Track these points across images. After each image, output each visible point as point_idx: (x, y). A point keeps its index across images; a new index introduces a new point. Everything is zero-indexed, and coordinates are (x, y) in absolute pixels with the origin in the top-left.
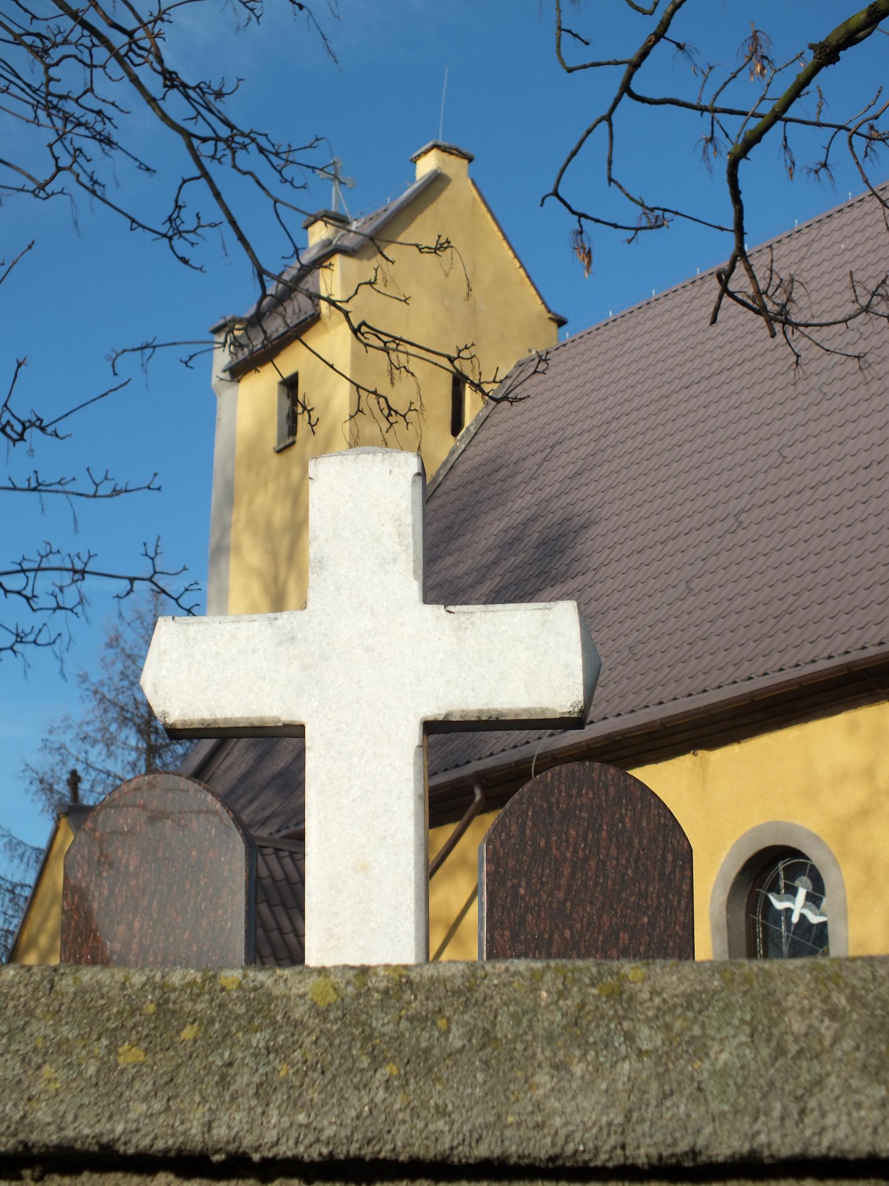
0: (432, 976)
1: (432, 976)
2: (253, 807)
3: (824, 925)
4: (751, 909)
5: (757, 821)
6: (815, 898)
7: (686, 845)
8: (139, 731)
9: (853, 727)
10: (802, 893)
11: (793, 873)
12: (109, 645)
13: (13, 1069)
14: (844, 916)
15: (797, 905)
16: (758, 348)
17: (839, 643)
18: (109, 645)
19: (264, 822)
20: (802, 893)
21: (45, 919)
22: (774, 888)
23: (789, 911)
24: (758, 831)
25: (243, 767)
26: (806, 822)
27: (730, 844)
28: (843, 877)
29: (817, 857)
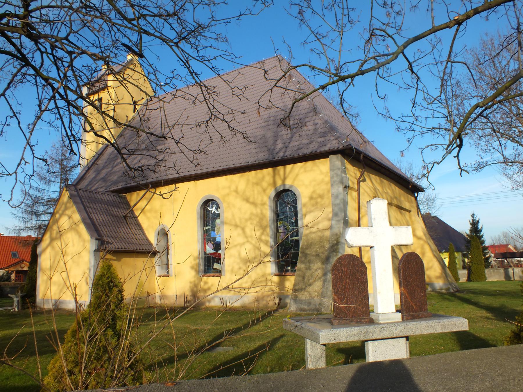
0: (513, 332)
1: (513, 332)
2: (97, 185)
3: (219, 214)
4: (204, 210)
5: (207, 194)
6: (217, 209)
7: (441, 313)
8: (60, 164)
9: (227, 179)
10: (214, 208)
11: (212, 204)
12: (52, 147)
13: (434, 304)
14: (223, 212)
15: (213, 210)
16: (229, 100)
17: (224, 164)
18: (52, 147)
19: (101, 188)
20: (214, 208)
21: (61, 208)
22: (209, 206)
23: (212, 211)
24: (207, 196)
25: (93, 176)
26: (216, 195)
27: (201, 198)
28: (224, 206)
29: (218, 202)
